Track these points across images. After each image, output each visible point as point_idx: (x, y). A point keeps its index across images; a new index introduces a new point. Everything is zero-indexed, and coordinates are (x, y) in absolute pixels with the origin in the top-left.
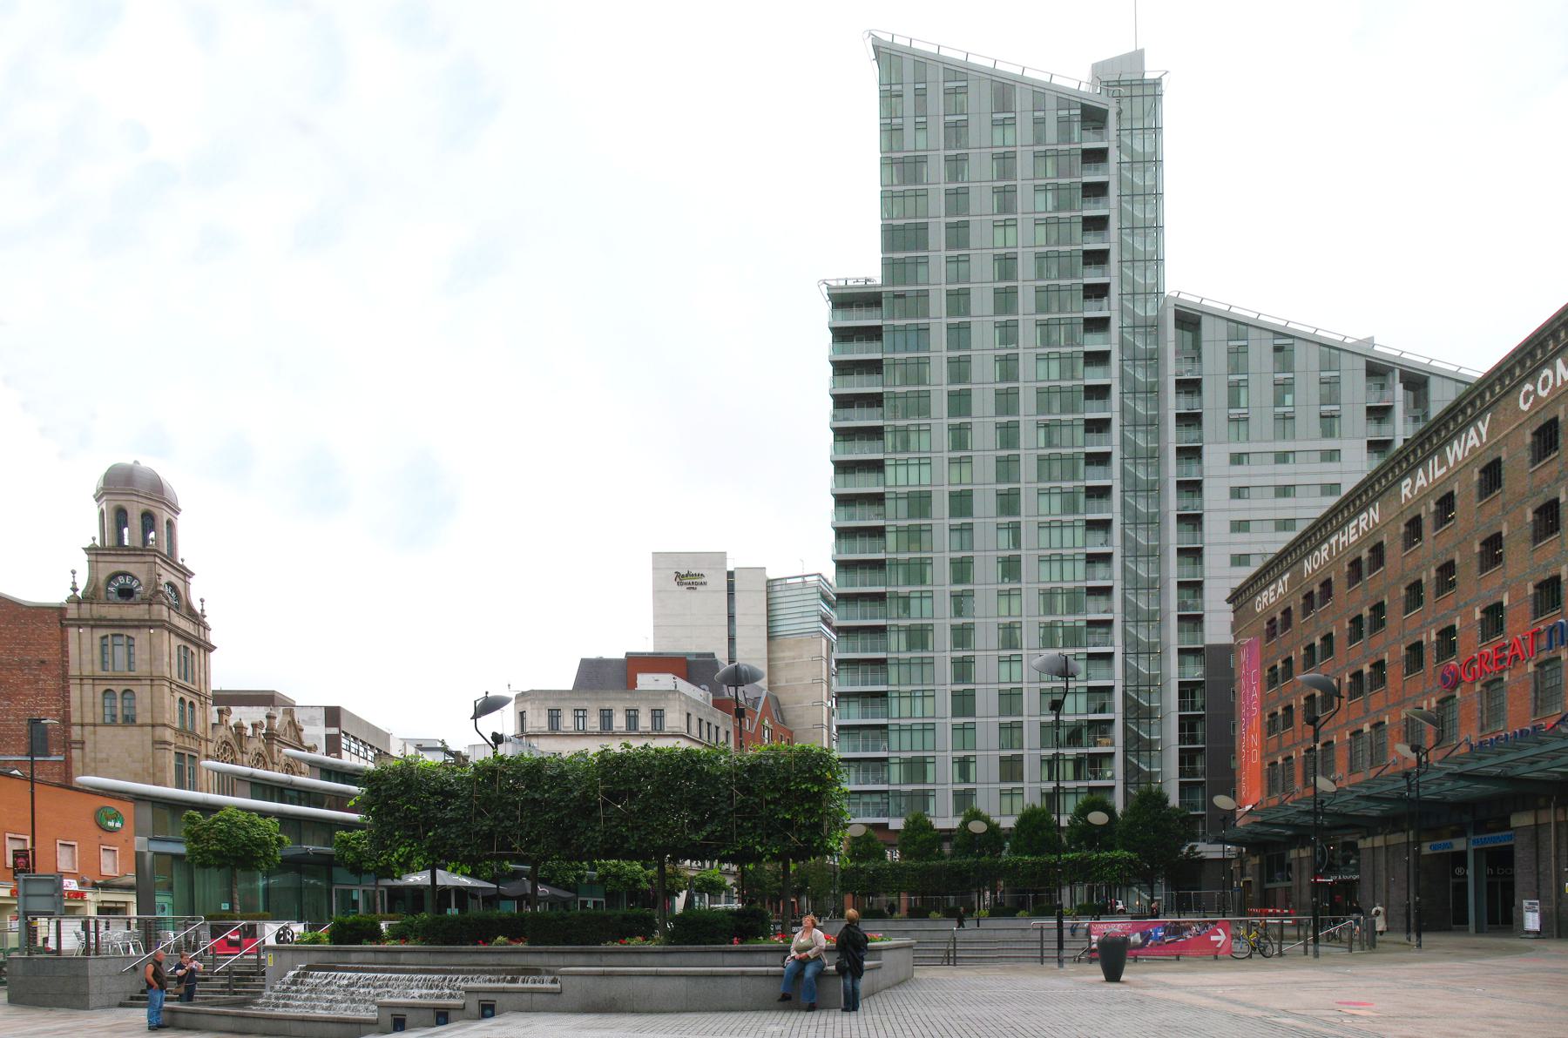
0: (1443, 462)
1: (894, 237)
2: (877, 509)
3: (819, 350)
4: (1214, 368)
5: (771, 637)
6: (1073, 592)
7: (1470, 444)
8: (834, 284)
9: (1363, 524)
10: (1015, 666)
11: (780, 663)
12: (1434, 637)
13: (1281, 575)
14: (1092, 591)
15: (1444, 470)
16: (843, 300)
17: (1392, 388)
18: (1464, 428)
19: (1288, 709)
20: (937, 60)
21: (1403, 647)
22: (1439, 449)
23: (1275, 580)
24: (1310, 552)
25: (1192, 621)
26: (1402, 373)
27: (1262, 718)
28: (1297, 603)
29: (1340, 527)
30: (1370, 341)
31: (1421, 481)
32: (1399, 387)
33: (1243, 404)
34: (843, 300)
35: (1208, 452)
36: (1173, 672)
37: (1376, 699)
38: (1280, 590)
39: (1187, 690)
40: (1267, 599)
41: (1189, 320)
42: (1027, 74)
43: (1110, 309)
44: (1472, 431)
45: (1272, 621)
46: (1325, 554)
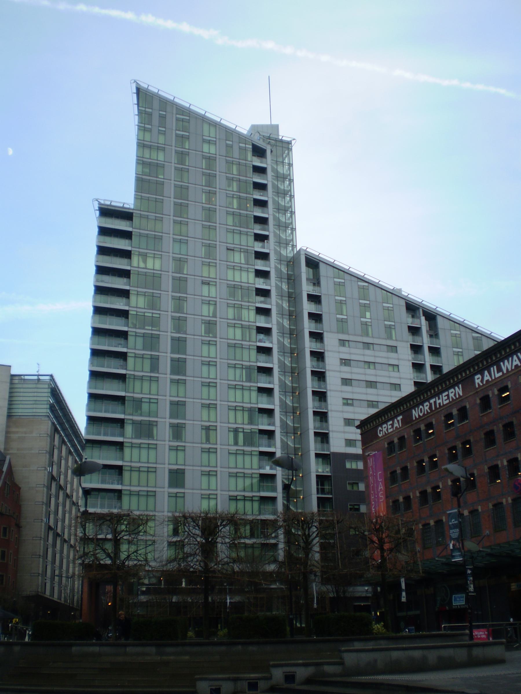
0: (499, 370)
1: (142, 184)
2: (122, 341)
3: (91, 240)
4: (326, 289)
5: (10, 416)
6: (250, 410)
7: (514, 363)
8: (102, 202)
9: (452, 395)
10: (212, 456)
11: (14, 436)
12: (505, 463)
13: (396, 417)
14: (262, 411)
15: (501, 374)
16: (106, 212)
17: (419, 318)
18: (511, 355)
19: (407, 499)
20: (173, 103)
21: (486, 467)
22: (497, 363)
23: (392, 419)
24: (417, 405)
25: (323, 437)
26: (423, 311)
27: (387, 503)
28: (409, 434)
29: (437, 395)
30: (400, 290)
31: (487, 377)
32: (423, 318)
33: (345, 313)
34: (106, 212)
35: (327, 336)
36: (315, 468)
37: (470, 497)
38: (396, 425)
39: (321, 479)
40: (385, 429)
41: (313, 263)
42: (222, 122)
43: (270, 247)
44: (515, 357)
45: (391, 443)
46: (427, 408)
